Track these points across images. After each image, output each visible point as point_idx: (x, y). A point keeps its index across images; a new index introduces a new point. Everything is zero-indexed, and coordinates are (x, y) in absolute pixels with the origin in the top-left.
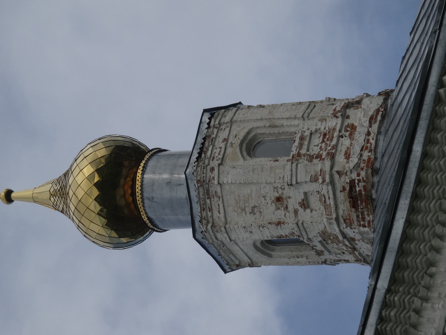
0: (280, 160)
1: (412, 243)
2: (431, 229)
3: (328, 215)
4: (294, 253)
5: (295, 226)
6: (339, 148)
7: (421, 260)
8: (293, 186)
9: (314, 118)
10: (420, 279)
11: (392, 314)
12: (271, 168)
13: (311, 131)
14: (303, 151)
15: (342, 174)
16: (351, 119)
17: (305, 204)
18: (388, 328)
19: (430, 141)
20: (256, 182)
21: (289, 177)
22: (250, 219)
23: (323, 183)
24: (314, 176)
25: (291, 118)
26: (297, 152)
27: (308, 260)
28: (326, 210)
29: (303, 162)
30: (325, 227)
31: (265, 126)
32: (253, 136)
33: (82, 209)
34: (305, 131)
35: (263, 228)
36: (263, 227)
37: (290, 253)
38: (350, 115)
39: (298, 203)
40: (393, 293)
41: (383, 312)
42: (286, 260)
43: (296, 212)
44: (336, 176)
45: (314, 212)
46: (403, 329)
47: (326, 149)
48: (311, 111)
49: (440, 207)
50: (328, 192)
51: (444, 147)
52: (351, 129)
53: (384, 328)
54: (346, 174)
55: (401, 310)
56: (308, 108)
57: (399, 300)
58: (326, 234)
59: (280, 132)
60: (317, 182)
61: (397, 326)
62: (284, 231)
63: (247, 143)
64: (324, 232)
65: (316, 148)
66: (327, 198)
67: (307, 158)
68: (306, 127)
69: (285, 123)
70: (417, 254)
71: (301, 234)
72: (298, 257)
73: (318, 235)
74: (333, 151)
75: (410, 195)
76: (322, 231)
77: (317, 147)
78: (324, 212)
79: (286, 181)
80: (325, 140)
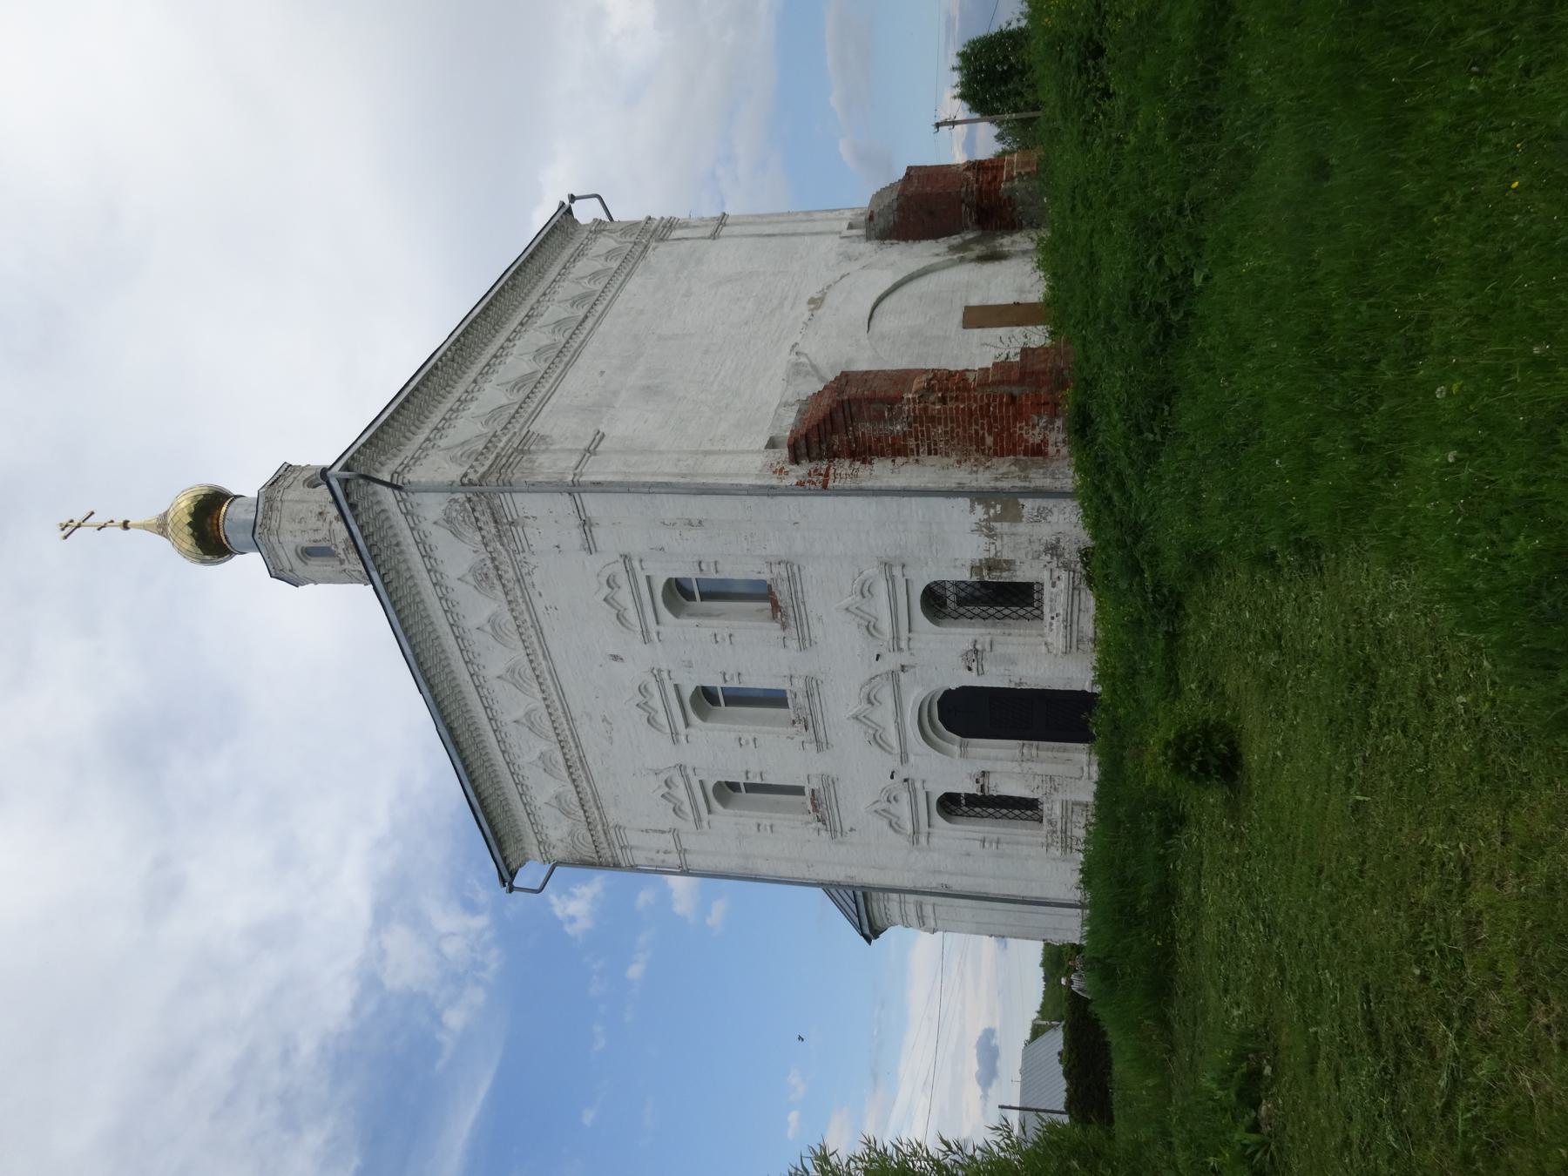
22: (297, 526)
43: (331, 523)
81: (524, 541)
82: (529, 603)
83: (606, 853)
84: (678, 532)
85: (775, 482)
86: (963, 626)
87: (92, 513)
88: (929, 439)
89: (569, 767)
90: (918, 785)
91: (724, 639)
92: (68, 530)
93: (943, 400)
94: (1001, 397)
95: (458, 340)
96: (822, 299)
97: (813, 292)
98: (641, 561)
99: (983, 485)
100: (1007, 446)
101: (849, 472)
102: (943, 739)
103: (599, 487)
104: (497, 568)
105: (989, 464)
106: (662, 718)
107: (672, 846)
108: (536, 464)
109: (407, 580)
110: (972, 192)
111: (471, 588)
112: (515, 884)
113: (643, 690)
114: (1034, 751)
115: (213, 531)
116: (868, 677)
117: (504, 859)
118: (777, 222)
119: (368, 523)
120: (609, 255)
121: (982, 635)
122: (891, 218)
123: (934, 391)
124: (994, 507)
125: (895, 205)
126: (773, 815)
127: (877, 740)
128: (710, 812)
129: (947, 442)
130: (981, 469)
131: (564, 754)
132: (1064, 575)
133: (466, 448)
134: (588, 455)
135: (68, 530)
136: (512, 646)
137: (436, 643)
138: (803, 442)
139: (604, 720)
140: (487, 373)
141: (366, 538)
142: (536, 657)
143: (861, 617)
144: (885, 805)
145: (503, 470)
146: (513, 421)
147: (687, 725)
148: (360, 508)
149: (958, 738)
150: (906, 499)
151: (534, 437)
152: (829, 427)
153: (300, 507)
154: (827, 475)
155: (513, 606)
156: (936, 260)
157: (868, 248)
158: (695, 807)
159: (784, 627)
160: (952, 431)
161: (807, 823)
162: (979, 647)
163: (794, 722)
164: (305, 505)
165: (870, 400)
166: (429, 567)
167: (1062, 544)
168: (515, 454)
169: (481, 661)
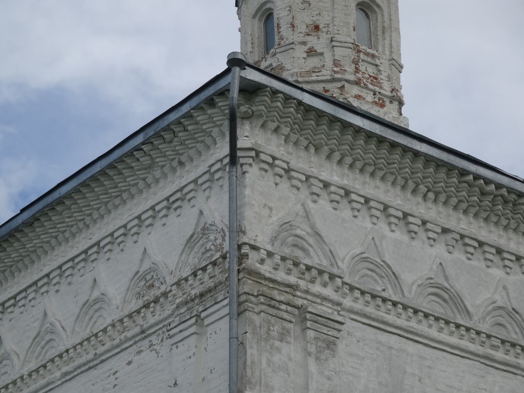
0: (354, 32)
1: (340, 132)
2: (349, 152)
3: (300, 74)
4: (256, 41)
5: (290, 41)
6: (364, 90)
7: (323, 139)
8: (330, 42)
9: (391, 69)
10: (305, 136)
11: (279, 104)
12: (348, 23)
13: (380, 66)
14: (362, 56)
15: (341, 90)
16: (390, 105)
17: (311, 52)
18: (266, 98)
19: (427, 161)
20: (335, 8)
21: (340, 40)
23: (333, 71)
24: (339, 63)
25: (391, 48)
26: (361, 49)
27: (249, 53)
28: (306, 73)
29: (353, 54)
30: (288, 70)
31: (384, 22)
32: (375, 10)
34: (379, 60)
35: (288, 10)
36: (290, 10)
37: (257, 37)
38: (393, 104)
39: (313, 45)
40: (297, 107)
41: (282, 94)
42: (249, 32)
43: (304, 43)
44: (339, 85)
45: (304, 60)
46: (263, 113)
47: (364, 78)
48: (396, 68)
49: (114, 231)
50: (324, 75)
51: (421, 174)
52: (380, 104)
53: (267, 94)
54: (341, 94)
55: (280, 113)
56: (399, 65)
57: (291, 113)
58: (280, 71)
59: (379, 37)
60: (334, 66)
61: (266, 108)
63: (369, 3)
64: (282, 69)
65: (364, 69)
66: (317, 74)
67: (356, 59)
68: (383, 61)
69: (387, 42)
70: (328, 136)
71: (281, 47)
72: (252, 44)
73: (280, 63)
74: (362, 85)
75: (384, 135)
76: (283, 67)
77: (365, 69)
78: (303, 70)
79: (335, 36)
80: (372, 78)
104: (156, 301)
108: (277, 343)
109: (144, 179)
111: (135, 269)
119: (197, 123)
133: (311, 240)
136: (77, 329)
137: (81, 225)
140: (466, 245)
141: (178, 122)
145: (262, 299)
146: (368, 297)
148: (209, 111)
151: (335, 333)
155: (119, 327)
166: (157, 208)
168: (296, 312)
169: (63, 288)
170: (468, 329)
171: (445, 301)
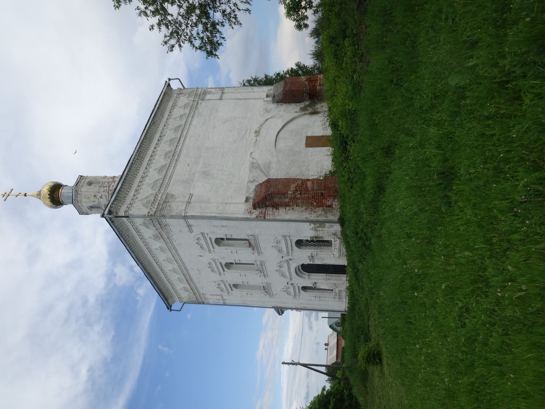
17: (101, 197)
22: (87, 200)
29: (102, 188)
33: (44, 196)
43: (99, 199)
62: (95, 203)
69: (99, 179)
81: (169, 230)
82: (172, 244)
83: (200, 300)
84: (219, 228)
85: (249, 216)
86: (308, 249)
87: (12, 190)
88: (296, 203)
89: (187, 281)
90: (296, 285)
91: (234, 252)
92: (5, 197)
93: (301, 194)
94: (318, 193)
95: (138, 150)
96: (259, 131)
97: (256, 128)
98: (207, 234)
99: (313, 219)
100: (320, 205)
101: (272, 213)
102: (303, 274)
103: (193, 217)
104: (161, 235)
105: (315, 210)
106: (216, 269)
107: (221, 298)
108: (172, 208)
109: (132, 238)
110: (307, 89)
112: (172, 308)
113: (210, 263)
114: (330, 277)
115: (57, 199)
116: (279, 261)
117: (168, 303)
118: (242, 92)
120: (185, 106)
121: (314, 252)
122: (281, 97)
123: (297, 191)
124: (317, 224)
125: (282, 93)
126: (252, 291)
127: (283, 275)
128: (232, 290)
129: (302, 204)
130: (313, 212)
131: (185, 278)
132: (338, 240)
133: (148, 199)
134: (188, 204)
135: (5, 197)
138: (257, 204)
139: (198, 270)
142: (175, 255)
143: (277, 248)
144: (286, 289)
145: (161, 211)
147: (224, 271)
149: (307, 273)
150: (290, 223)
151: (170, 195)
152: (265, 200)
153: (87, 193)
154: (265, 214)
156: (296, 114)
157: (273, 106)
158: (227, 289)
159: (253, 250)
160: (303, 201)
161: (262, 293)
162: (313, 255)
163: (257, 270)
164: (89, 193)
165: (278, 194)
167: (337, 233)
169: (157, 256)
170: (170, 164)
171: (163, 169)
